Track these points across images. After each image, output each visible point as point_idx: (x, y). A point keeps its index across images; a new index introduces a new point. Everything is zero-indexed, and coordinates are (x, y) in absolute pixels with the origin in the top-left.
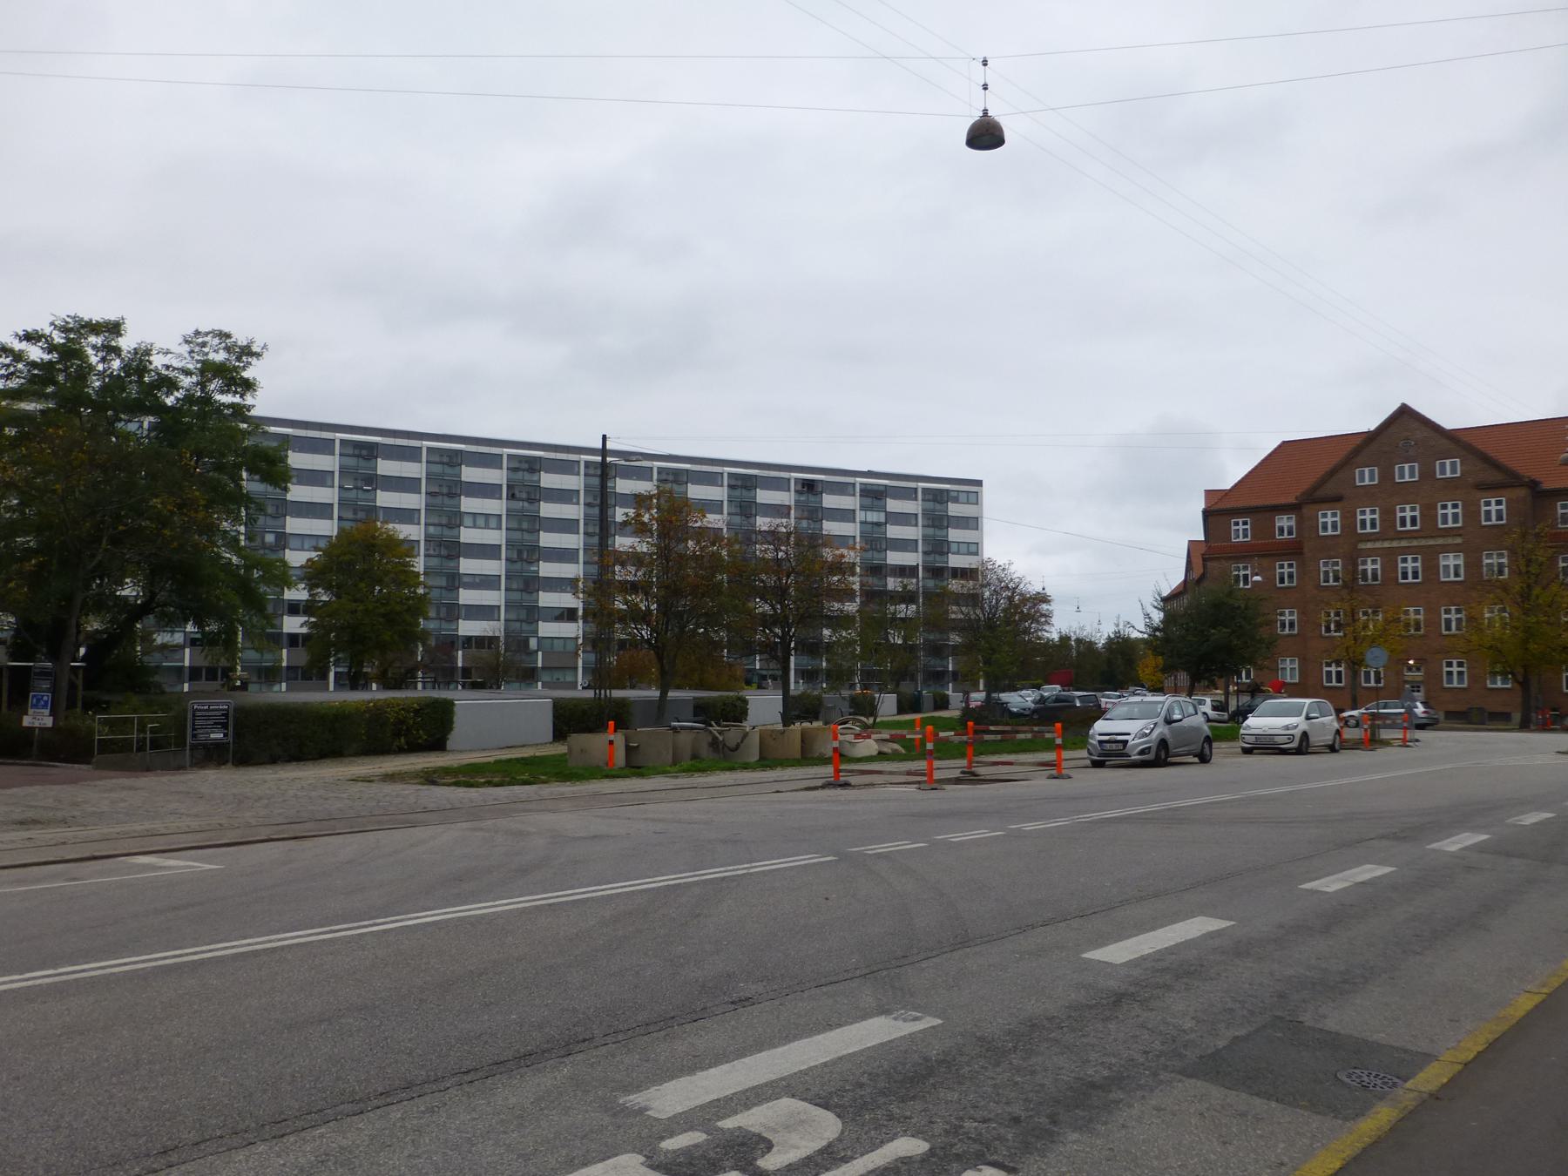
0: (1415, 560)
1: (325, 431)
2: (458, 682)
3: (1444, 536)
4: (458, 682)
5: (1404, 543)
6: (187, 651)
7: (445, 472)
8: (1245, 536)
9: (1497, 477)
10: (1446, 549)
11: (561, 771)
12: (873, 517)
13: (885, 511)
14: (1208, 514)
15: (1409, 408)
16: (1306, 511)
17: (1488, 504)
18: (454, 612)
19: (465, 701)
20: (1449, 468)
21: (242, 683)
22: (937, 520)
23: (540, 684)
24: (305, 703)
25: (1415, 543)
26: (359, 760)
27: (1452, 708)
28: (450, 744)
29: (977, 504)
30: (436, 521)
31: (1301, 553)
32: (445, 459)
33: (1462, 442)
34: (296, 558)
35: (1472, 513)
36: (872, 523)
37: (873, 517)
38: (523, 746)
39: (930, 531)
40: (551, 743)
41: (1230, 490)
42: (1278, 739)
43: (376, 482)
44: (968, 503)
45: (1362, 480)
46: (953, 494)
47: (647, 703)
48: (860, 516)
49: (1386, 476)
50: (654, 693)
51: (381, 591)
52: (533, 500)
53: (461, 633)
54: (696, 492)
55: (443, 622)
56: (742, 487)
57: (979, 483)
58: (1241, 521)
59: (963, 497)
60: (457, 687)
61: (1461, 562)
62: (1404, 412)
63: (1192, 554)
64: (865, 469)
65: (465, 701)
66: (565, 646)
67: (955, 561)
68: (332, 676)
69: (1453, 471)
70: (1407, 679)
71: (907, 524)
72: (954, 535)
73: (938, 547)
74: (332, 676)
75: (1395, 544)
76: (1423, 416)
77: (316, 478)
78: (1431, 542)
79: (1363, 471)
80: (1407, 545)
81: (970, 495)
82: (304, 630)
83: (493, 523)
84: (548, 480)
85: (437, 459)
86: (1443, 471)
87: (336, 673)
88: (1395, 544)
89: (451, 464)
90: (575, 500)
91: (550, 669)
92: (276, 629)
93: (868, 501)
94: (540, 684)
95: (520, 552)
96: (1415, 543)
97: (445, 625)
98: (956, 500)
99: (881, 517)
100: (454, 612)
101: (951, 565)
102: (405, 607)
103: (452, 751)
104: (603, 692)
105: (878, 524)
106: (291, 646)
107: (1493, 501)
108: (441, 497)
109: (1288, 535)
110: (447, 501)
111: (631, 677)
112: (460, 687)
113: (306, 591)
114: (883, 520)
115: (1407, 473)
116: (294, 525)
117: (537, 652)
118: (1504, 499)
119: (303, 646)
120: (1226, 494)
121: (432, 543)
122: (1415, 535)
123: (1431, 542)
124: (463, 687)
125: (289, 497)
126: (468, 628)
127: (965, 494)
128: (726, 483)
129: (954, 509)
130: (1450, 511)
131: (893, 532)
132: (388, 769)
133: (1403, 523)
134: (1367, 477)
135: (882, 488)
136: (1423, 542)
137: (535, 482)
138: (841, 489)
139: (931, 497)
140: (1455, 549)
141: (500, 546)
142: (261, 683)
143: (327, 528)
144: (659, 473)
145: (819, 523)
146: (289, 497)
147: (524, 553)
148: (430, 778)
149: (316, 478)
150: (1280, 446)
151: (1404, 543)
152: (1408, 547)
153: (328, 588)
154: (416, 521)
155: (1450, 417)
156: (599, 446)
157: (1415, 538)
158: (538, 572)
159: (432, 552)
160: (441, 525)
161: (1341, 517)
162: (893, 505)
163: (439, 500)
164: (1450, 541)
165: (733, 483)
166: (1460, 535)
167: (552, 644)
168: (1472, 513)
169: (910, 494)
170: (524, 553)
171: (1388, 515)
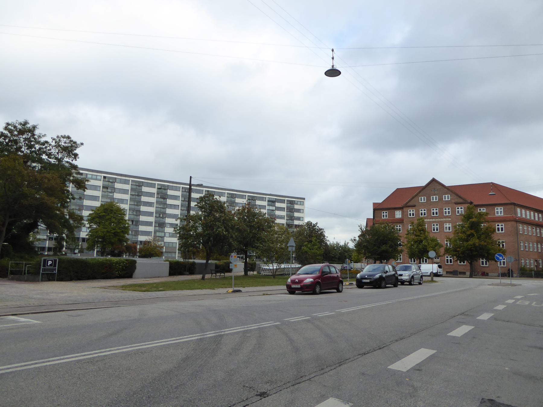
0: (437, 225)
1: (94, 172)
2: (137, 256)
3: (445, 218)
4: (137, 256)
5: (434, 220)
6: (47, 242)
7: (137, 188)
8: (386, 217)
10: (446, 222)
11: (166, 287)
12: (271, 208)
14: (375, 210)
15: (435, 179)
16: (405, 209)
17: (458, 208)
18: (137, 233)
19: (140, 261)
20: (447, 197)
21: (65, 253)
22: (291, 210)
23: (164, 257)
25: (437, 220)
26: (102, 280)
27: (448, 270)
28: (134, 275)
30: (133, 204)
31: (403, 222)
32: (137, 184)
34: (86, 213)
35: (454, 212)
37: (271, 208)
38: (159, 277)
39: (289, 213)
40: (168, 277)
41: (382, 203)
43: (114, 190)
44: (300, 205)
45: (421, 200)
46: (296, 202)
47: (201, 264)
48: (267, 207)
49: (428, 199)
50: (204, 261)
51: (113, 225)
52: (164, 198)
53: (139, 240)
54: (258, 203)
55: (133, 236)
56: (231, 197)
57: (304, 199)
58: (385, 212)
59: (299, 203)
60: (137, 257)
61: (450, 226)
62: (434, 181)
63: (368, 223)
64: (269, 193)
65: (140, 261)
67: (296, 222)
68: (95, 251)
69: (448, 198)
70: (434, 261)
71: (96, 190)
72: (296, 214)
73: (291, 218)
74: (95, 251)
75: (431, 220)
76: (438, 181)
77: (175, 198)
78: (442, 220)
79: (422, 198)
80: (434, 220)
82: (87, 237)
83: (125, 202)
84: (170, 192)
85: (135, 184)
86: (445, 198)
87: (97, 251)
88: (431, 220)
89: (139, 186)
90: (178, 199)
91: (167, 252)
93: (270, 203)
94: (164, 257)
95: (160, 215)
96: (437, 220)
97: (134, 237)
98: (297, 204)
99: (274, 208)
100: (137, 233)
102: (121, 231)
103: (135, 278)
104: (186, 260)
105: (273, 210)
106: (83, 242)
107: (460, 208)
108: (135, 196)
110: (137, 197)
111: (195, 254)
112: (138, 257)
113: (88, 224)
114: (274, 209)
115: (434, 199)
116: (86, 203)
117: (163, 246)
118: (463, 207)
119: (86, 242)
120: (380, 204)
121: (131, 210)
122: (438, 217)
123: (442, 220)
124: (139, 257)
125: (85, 193)
126: (142, 238)
128: (226, 196)
129: (296, 207)
130: (447, 210)
131: (278, 213)
133: (433, 214)
134: (422, 199)
135: (274, 200)
136: (439, 220)
137: (166, 193)
138: (262, 199)
139: (289, 203)
140: (449, 222)
141: (153, 212)
142: (72, 253)
143: (97, 204)
144: (205, 192)
145: (113, 193)
146: (85, 193)
147: (161, 214)
148: (124, 287)
149: (175, 198)
150: (396, 190)
151: (434, 220)
152: (435, 221)
153: (95, 223)
154: (153, 206)
155: (448, 182)
156: (189, 183)
157: (437, 218)
159: (131, 213)
160: (134, 205)
161: (415, 212)
162: (278, 205)
163: (134, 197)
164: (447, 219)
165: (228, 196)
166: (450, 218)
167: (169, 244)
168: (454, 212)
169: (283, 201)
170: (161, 214)
171: (429, 211)
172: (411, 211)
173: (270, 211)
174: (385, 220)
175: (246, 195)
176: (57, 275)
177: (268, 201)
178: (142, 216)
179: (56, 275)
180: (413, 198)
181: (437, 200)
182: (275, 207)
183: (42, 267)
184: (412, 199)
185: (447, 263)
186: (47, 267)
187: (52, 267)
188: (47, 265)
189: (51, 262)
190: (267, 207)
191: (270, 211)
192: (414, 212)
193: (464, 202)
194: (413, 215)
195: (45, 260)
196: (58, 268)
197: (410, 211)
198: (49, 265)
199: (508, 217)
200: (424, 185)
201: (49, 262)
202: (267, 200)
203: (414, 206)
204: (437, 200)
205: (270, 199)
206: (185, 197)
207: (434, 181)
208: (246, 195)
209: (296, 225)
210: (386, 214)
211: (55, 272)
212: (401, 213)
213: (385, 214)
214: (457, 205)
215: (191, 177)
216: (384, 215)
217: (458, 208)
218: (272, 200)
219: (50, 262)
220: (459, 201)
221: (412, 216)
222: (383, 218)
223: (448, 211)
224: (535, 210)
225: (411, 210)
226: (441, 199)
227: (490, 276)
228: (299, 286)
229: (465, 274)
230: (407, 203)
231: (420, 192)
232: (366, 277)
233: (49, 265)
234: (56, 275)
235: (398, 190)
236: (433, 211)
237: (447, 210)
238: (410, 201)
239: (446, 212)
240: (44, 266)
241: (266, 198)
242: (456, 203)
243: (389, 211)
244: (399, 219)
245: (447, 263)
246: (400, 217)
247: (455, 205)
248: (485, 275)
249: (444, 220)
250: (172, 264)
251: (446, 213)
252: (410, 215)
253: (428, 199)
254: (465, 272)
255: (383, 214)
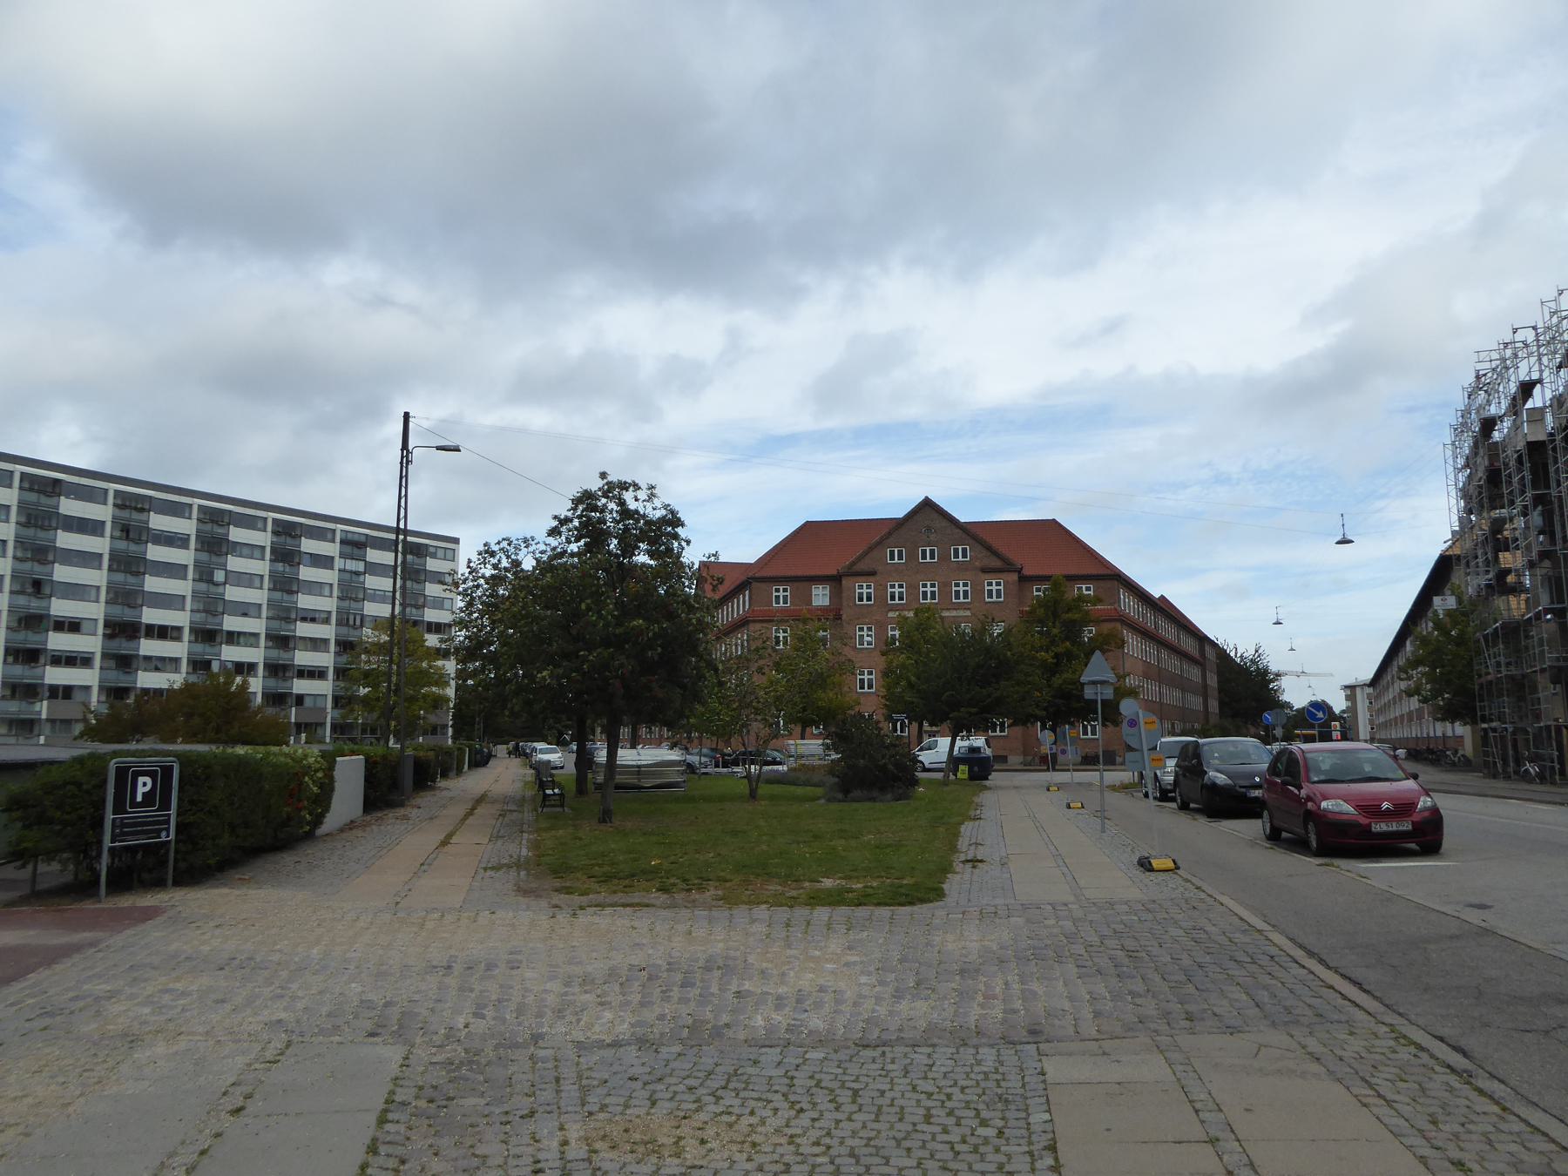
9: (997, 563)
13: (226, 570)
24: (82, 901)
29: (453, 561)
33: (975, 534)
35: (978, 591)
36: (351, 572)
42: (557, 763)
46: (432, 550)
49: (912, 556)
57: (456, 541)
59: (440, 553)
62: (927, 505)
66: (315, 703)
81: (447, 551)
92: (1041, 731)
93: (348, 549)
98: (434, 556)
99: (360, 567)
101: (427, 619)
105: (357, 573)
109: (867, 601)
127: (443, 550)
129: (432, 565)
132: (47, 972)
134: (895, 557)
135: (363, 539)
158: (224, 594)
166: (969, 609)
168: (978, 591)
172: (864, 588)
173: (347, 576)
174: (782, 610)
175: (266, 519)
176: (176, 852)
177: (342, 542)
178: (371, 548)
179: (172, 854)
180: (871, 549)
181: (936, 560)
182: (363, 562)
183: (110, 816)
184: (866, 554)
185: (1083, 735)
186: (132, 813)
187: (151, 812)
188: (134, 804)
189: (148, 780)
190: (339, 563)
191: (347, 576)
192: (871, 591)
193: (1007, 567)
194: (869, 599)
195: (121, 772)
196: (178, 815)
197: (861, 587)
198: (139, 799)
199: (1104, 609)
200: (901, 517)
201: (141, 780)
202: (338, 539)
203: (872, 573)
204: (936, 560)
205: (350, 536)
206: (30, 511)
207: (927, 505)
208: (266, 519)
209: (430, 624)
210: (785, 594)
211: (168, 836)
212: (827, 592)
213: (781, 594)
214: (987, 576)
215: (407, 416)
216: (778, 597)
217: (990, 584)
218: (356, 538)
219: (145, 784)
220: (993, 564)
221: (865, 602)
222: (774, 605)
223: (997, 590)
224: (1139, 593)
225: (865, 584)
226: (944, 557)
227: (1060, 765)
228: (1406, 826)
229: (1006, 762)
230: (853, 564)
231: (890, 534)
232: (1257, 779)
233: (139, 799)
234: (172, 854)
235: (808, 525)
236: (924, 589)
237: (961, 589)
238: (859, 559)
239: (957, 593)
240: (119, 807)
241: (334, 531)
242: (985, 570)
243: (796, 584)
244: (823, 609)
245: (1083, 735)
246: (826, 602)
247: (983, 576)
248: (1049, 763)
249: (952, 615)
250: (375, 763)
251: (957, 597)
252: (861, 599)
253: (912, 556)
254: (1006, 757)
255: (775, 594)
